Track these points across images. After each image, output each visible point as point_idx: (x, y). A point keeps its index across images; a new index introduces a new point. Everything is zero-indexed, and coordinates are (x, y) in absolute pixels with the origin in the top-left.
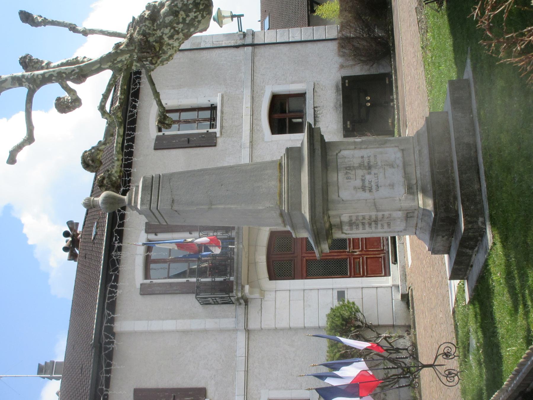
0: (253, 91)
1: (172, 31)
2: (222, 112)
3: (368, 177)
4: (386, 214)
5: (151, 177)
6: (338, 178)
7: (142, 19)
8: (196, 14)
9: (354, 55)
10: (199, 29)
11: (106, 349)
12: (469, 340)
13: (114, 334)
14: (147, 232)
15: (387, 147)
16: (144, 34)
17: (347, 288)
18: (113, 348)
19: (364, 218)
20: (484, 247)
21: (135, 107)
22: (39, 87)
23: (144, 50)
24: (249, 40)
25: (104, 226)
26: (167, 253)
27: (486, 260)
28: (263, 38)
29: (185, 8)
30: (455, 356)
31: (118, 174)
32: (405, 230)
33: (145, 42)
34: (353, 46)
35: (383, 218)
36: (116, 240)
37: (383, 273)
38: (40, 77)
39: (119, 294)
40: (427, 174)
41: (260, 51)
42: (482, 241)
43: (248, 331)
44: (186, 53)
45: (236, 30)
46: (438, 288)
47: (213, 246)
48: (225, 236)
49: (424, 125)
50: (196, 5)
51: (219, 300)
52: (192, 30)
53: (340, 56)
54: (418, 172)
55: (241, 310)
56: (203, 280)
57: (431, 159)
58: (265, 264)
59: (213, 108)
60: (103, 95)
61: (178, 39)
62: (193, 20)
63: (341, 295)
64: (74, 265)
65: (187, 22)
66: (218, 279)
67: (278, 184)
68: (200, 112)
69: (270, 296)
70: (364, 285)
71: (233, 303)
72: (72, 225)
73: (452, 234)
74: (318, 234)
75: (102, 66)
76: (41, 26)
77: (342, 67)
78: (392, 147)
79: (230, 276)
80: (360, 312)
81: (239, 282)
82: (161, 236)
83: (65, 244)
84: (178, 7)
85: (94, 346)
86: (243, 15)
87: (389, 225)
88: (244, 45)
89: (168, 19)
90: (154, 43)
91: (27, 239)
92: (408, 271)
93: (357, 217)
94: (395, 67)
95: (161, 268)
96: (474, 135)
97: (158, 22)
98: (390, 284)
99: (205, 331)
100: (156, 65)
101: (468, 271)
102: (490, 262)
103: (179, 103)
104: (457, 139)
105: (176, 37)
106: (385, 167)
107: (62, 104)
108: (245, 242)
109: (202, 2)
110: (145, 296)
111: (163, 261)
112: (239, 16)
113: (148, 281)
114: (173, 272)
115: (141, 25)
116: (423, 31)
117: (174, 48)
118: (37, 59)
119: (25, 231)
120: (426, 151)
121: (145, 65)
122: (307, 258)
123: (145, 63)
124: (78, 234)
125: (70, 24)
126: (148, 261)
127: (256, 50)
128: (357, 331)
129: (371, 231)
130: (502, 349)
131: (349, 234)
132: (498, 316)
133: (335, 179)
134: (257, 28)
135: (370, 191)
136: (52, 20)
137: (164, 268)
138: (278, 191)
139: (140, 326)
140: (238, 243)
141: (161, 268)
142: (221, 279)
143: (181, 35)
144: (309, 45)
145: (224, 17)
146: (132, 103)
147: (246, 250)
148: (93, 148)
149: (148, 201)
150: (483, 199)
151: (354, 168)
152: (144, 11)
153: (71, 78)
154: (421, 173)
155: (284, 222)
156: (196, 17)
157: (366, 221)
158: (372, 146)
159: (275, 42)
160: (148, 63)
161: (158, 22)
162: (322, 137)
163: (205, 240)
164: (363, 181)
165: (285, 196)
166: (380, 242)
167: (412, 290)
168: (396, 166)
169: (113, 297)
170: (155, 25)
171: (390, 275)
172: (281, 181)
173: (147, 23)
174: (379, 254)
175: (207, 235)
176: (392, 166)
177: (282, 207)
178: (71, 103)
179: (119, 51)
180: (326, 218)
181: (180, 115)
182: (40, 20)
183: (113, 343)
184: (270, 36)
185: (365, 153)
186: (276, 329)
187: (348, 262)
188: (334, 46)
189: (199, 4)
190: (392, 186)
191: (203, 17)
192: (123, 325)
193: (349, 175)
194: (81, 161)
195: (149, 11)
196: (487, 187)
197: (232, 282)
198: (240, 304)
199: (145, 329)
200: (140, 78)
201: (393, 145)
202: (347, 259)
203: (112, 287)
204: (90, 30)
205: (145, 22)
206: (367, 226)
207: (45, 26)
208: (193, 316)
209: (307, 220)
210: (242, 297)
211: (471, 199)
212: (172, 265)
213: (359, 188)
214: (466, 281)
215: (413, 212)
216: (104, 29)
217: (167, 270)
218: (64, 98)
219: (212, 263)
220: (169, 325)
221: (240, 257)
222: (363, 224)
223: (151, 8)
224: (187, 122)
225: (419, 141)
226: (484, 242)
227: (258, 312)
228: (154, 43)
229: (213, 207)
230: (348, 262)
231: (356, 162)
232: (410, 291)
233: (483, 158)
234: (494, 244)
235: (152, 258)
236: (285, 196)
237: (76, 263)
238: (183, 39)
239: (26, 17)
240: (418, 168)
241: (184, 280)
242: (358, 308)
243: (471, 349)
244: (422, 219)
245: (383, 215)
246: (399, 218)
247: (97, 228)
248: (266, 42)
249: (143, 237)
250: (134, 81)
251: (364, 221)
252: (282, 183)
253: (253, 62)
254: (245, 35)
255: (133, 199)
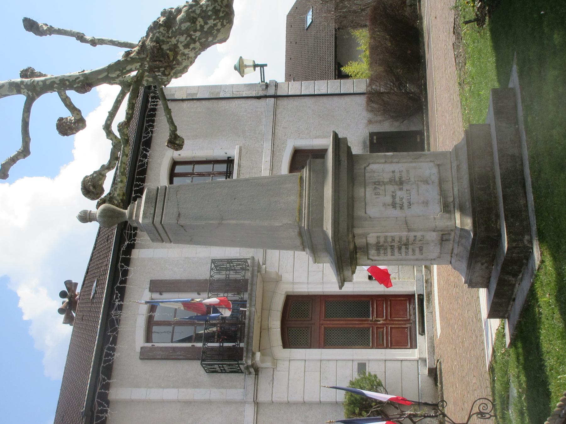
0: (273, 144)
1: (188, 39)
2: (239, 166)
3: (399, 194)
4: (419, 234)
5: (156, 188)
6: (366, 194)
7: (157, 25)
8: (215, 22)
9: (384, 110)
10: (218, 39)
11: (98, 418)
12: (508, 392)
13: (108, 402)
14: (151, 290)
15: (421, 162)
16: (158, 41)
17: (369, 360)
18: (106, 418)
19: (393, 240)
20: (530, 270)
21: (145, 156)
22: (39, 95)
23: (156, 59)
24: (271, 92)
25: (104, 284)
26: (172, 314)
27: (533, 285)
28: (286, 89)
29: (203, 14)
30: (491, 416)
31: (121, 197)
32: (439, 257)
33: (158, 50)
34: (383, 100)
35: (414, 240)
36: (117, 298)
37: (409, 344)
38: (41, 83)
39: (117, 357)
40: (466, 191)
41: (283, 103)
42: (527, 265)
43: (257, 404)
44: (204, 102)
45: (258, 80)
46: (472, 351)
47: (223, 308)
48: (237, 298)
49: (463, 139)
50: (216, 12)
51: (226, 368)
52: (210, 39)
53: (367, 110)
54: (456, 189)
55: (250, 380)
56: (210, 345)
57: (470, 174)
58: (279, 330)
59: (229, 161)
60: (109, 112)
61: (194, 49)
62: (212, 28)
63: (362, 367)
64: (69, 329)
65: (205, 30)
66: (226, 345)
67: (298, 199)
68: (215, 165)
69: (282, 366)
70: (388, 357)
71: (242, 372)
72: (70, 285)
73: (493, 260)
74: (341, 257)
75: (110, 75)
76: (46, 35)
77: (370, 122)
78: (427, 162)
79: (240, 342)
80: (382, 386)
81: (250, 348)
82: (167, 296)
83: (60, 306)
84: (196, 14)
85: (85, 414)
86: (266, 65)
87: (421, 249)
88: (266, 97)
89: (185, 26)
90: (168, 52)
91: (22, 314)
92: (436, 342)
93: (386, 237)
94: (427, 122)
95: (165, 332)
96: (520, 146)
97: (174, 29)
98: (416, 357)
99: (210, 402)
100: (169, 77)
101: (510, 306)
102: (537, 285)
103: (194, 155)
104: (500, 150)
105: (192, 46)
106: (419, 183)
107: (64, 124)
108: (259, 306)
109: (222, 9)
110: (145, 361)
111: (168, 323)
112: (262, 66)
113: (149, 345)
114: (177, 337)
115: (155, 31)
116: (460, 62)
117: (190, 59)
118: (40, 72)
119: (21, 304)
120: (465, 167)
121: (157, 76)
122: (326, 326)
123: (157, 74)
124: (77, 296)
125: (78, 33)
126: (150, 323)
127: (279, 102)
128: (378, 407)
129: (400, 257)
130: (550, 384)
131: (375, 260)
132: (545, 346)
133: (363, 194)
134: (280, 78)
135: (401, 208)
136: (59, 29)
137: (168, 332)
138: (297, 207)
139: (138, 394)
140: (250, 306)
141: (165, 332)
142: (231, 344)
143: (198, 44)
144: (336, 99)
145: (246, 66)
146: (142, 152)
147: (259, 314)
148: (95, 172)
149: (150, 214)
150: (530, 214)
151: (384, 184)
152: (159, 18)
153: (75, 86)
154: (458, 190)
155: (303, 243)
156: (215, 25)
157: (396, 244)
158: (405, 161)
159: (299, 94)
160: (160, 74)
161: (174, 29)
162: (349, 148)
163: (214, 300)
164: (394, 197)
165: (305, 212)
166: (406, 311)
167: (440, 363)
168: (430, 182)
169: (110, 360)
170: (170, 32)
171: (416, 348)
172: (301, 196)
173: (162, 29)
174: (405, 324)
175: (217, 296)
176: (426, 182)
177: (301, 224)
178: (75, 123)
179: (129, 59)
180: (351, 236)
181: (194, 168)
182: (45, 28)
183: (106, 411)
184: (295, 88)
185: (396, 167)
186: (288, 403)
187: (371, 331)
188: (362, 100)
189: (219, 11)
190: (426, 203)
191: (223, 25)
192: (118, 393)
193: (378, 191)
194: (81, 187)
195: (164, 17)
196: (534, 199)
197: (242, 348)
198: (250, 373)
199: (144, 397)
200: (153, 126)
201: (428, 160)
202: (369, 328)
203: (109, 349)
204: (99, 40)
205: (159, 28)
206: (396, 250)
207: (50, 35)
208: (196, 385)
209: (329, 239)
210: (252, 366)
211: (516, 216)
212: (177, 328)
213: (389, 205)
214: (507, 320)
215: (449, 234)
216: (114, 39)
217: (171, 334)
218: (67, 118)
219: (221, 328)
220: (171, 394)
221: (252, 320)
222: (392, 247)
223: (167, 15)
224: (200, 175)
225: (457, 156)
226: (530, 265)
227: (269, 383)
228: (168, 52)
229: (223, 222)
230: (371, 331)
231: (386, 177)
232: (438, 364)
233: (531, 168)
234: (542, 262)
235: (155, 319)
236: (305, 212)
237: (72, 327)
238: (200, 50)
239: (31, 25)
240: (456, 184)
241: (189, 345)
242: (380, 382)
243: (511, 400)
244: (459, 242)
245: (415, 236)
246: (433, 241)
247: (97, 286)
248: (290, 94)
249: (147, 296)
250: (147, 129)
251: (393, 244)
252: (302, 198)
253: (275, 115)
254: (267, 86)
255: (135, 213)
